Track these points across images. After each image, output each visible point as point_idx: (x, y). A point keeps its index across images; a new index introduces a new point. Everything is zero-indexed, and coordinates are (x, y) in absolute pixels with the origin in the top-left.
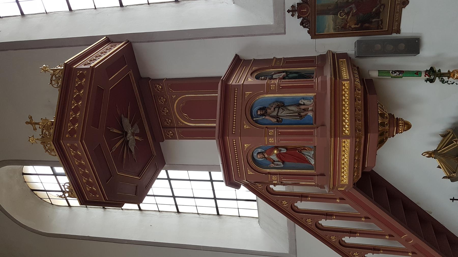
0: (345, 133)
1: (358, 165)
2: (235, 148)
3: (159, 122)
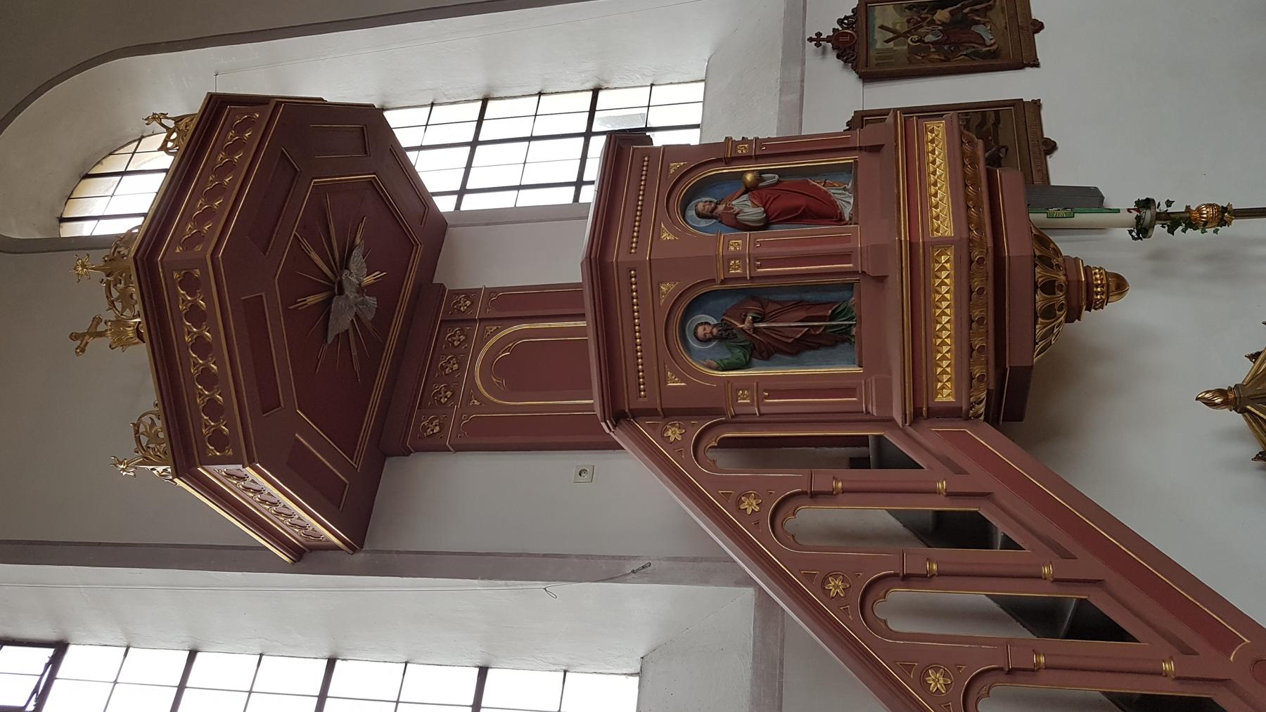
0: (939, 255)
1: (979, 213)
2: (634, 231)
3: (416, 396)
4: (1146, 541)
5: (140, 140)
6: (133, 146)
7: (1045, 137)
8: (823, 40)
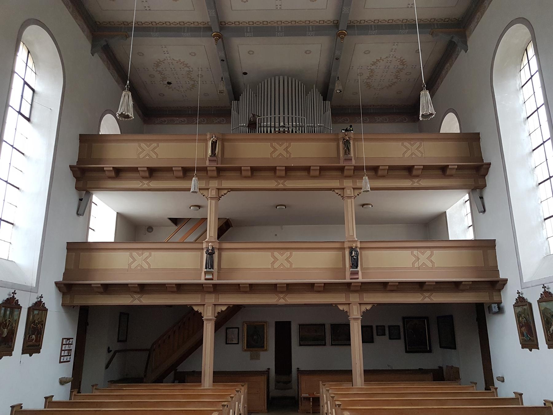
4: (363, 352)
5: (35, 73)
6: (34, 69)
7: (532, 349)
8: (41, 298)
